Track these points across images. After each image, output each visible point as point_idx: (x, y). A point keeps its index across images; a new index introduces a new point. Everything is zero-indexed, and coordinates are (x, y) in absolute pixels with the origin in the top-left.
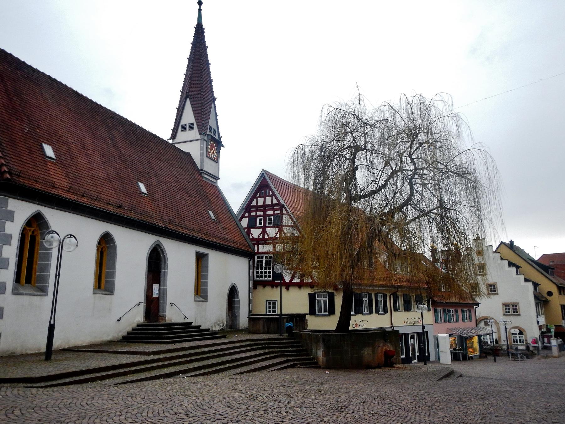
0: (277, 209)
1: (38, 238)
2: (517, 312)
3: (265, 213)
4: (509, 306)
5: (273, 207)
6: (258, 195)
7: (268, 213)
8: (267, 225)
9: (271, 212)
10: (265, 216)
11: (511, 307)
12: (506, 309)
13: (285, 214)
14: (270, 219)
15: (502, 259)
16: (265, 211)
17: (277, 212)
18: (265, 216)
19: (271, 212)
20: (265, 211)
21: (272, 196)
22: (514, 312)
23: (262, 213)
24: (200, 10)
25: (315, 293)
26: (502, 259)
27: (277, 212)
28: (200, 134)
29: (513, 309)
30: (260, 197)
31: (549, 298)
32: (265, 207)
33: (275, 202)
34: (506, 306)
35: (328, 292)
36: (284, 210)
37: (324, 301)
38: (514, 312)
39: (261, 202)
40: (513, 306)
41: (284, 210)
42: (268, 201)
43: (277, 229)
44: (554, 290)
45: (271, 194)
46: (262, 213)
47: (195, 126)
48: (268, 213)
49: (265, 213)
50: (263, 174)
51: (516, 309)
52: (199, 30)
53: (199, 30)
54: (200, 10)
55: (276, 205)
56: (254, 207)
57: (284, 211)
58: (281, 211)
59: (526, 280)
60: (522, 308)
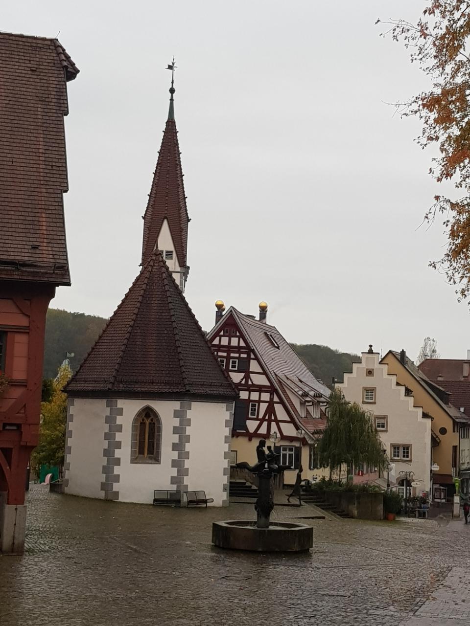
0: (244, 353)
1: (389, 473)
2: (408, 457)
3: (228, 355)
4: (398, 448)
5: (238, 349)
6: (222, 333)
7: (232, 355)
8: (230, 368)
9: (237, 355)
10: (228, 358)
11: (401, 450)
12: (395, 452)
13: (253, 359)
14: (234, 362)
15: (398, 384)
16: (229, 353)
17: (244, 356)
18: (228, 358)
19: (237, 355)
20: (229, 353)
21: (239, 337)
22: (404, 456)
23: (225, 354)
24: (172, 100)
25: (281, 446)
26: (398, 384)
27: (244, 356)
28: (180, 266)
29: (404, 452)
30: (224, 336)
31: (441, 436)
32: (229, 348)
33: (242, 344)
34: (395, 448)
35: (295, 446)
36: (252, 354)
37: (290, 456)
38: (404, 456)
39: (225, 341)
40: (404, 449)
41: (252, 354)
42: (234, 342)
43: (243, 374)
44: (449, 426)
45: (238, 334)
46: (225, 354)
47: (174, 255)
48: (232, 355)
49: (228, 355)
50: (231, 311)
51: (408, 452)
52: (171, 125)
53: (171, 125)
54: (172, 100)
55: (243, 348)
56: (215, 346)
57: (252, 356)
58: (249, 355)
59: (425, 415)
60: (414, 453)
